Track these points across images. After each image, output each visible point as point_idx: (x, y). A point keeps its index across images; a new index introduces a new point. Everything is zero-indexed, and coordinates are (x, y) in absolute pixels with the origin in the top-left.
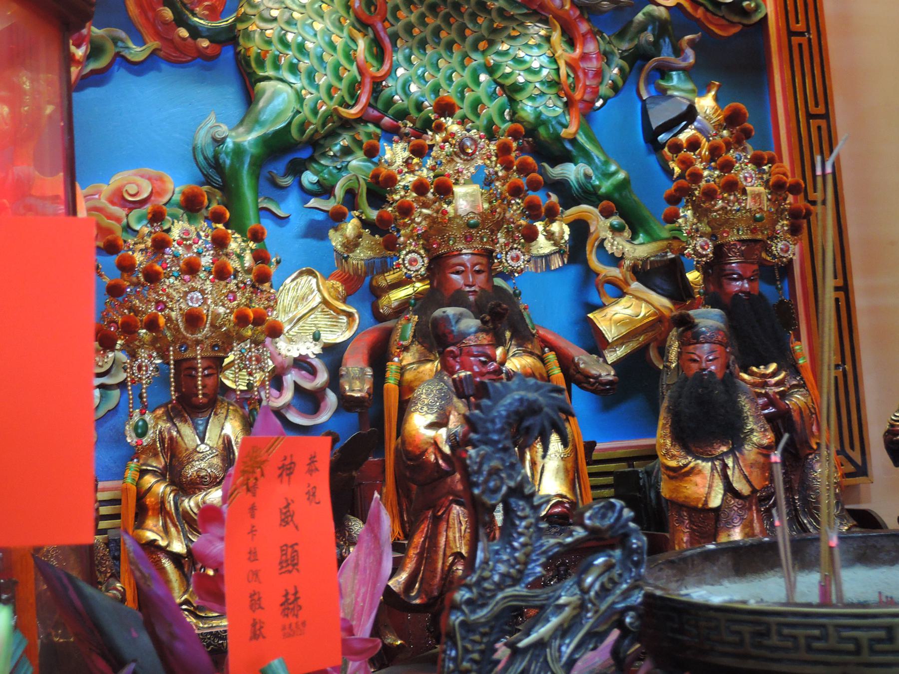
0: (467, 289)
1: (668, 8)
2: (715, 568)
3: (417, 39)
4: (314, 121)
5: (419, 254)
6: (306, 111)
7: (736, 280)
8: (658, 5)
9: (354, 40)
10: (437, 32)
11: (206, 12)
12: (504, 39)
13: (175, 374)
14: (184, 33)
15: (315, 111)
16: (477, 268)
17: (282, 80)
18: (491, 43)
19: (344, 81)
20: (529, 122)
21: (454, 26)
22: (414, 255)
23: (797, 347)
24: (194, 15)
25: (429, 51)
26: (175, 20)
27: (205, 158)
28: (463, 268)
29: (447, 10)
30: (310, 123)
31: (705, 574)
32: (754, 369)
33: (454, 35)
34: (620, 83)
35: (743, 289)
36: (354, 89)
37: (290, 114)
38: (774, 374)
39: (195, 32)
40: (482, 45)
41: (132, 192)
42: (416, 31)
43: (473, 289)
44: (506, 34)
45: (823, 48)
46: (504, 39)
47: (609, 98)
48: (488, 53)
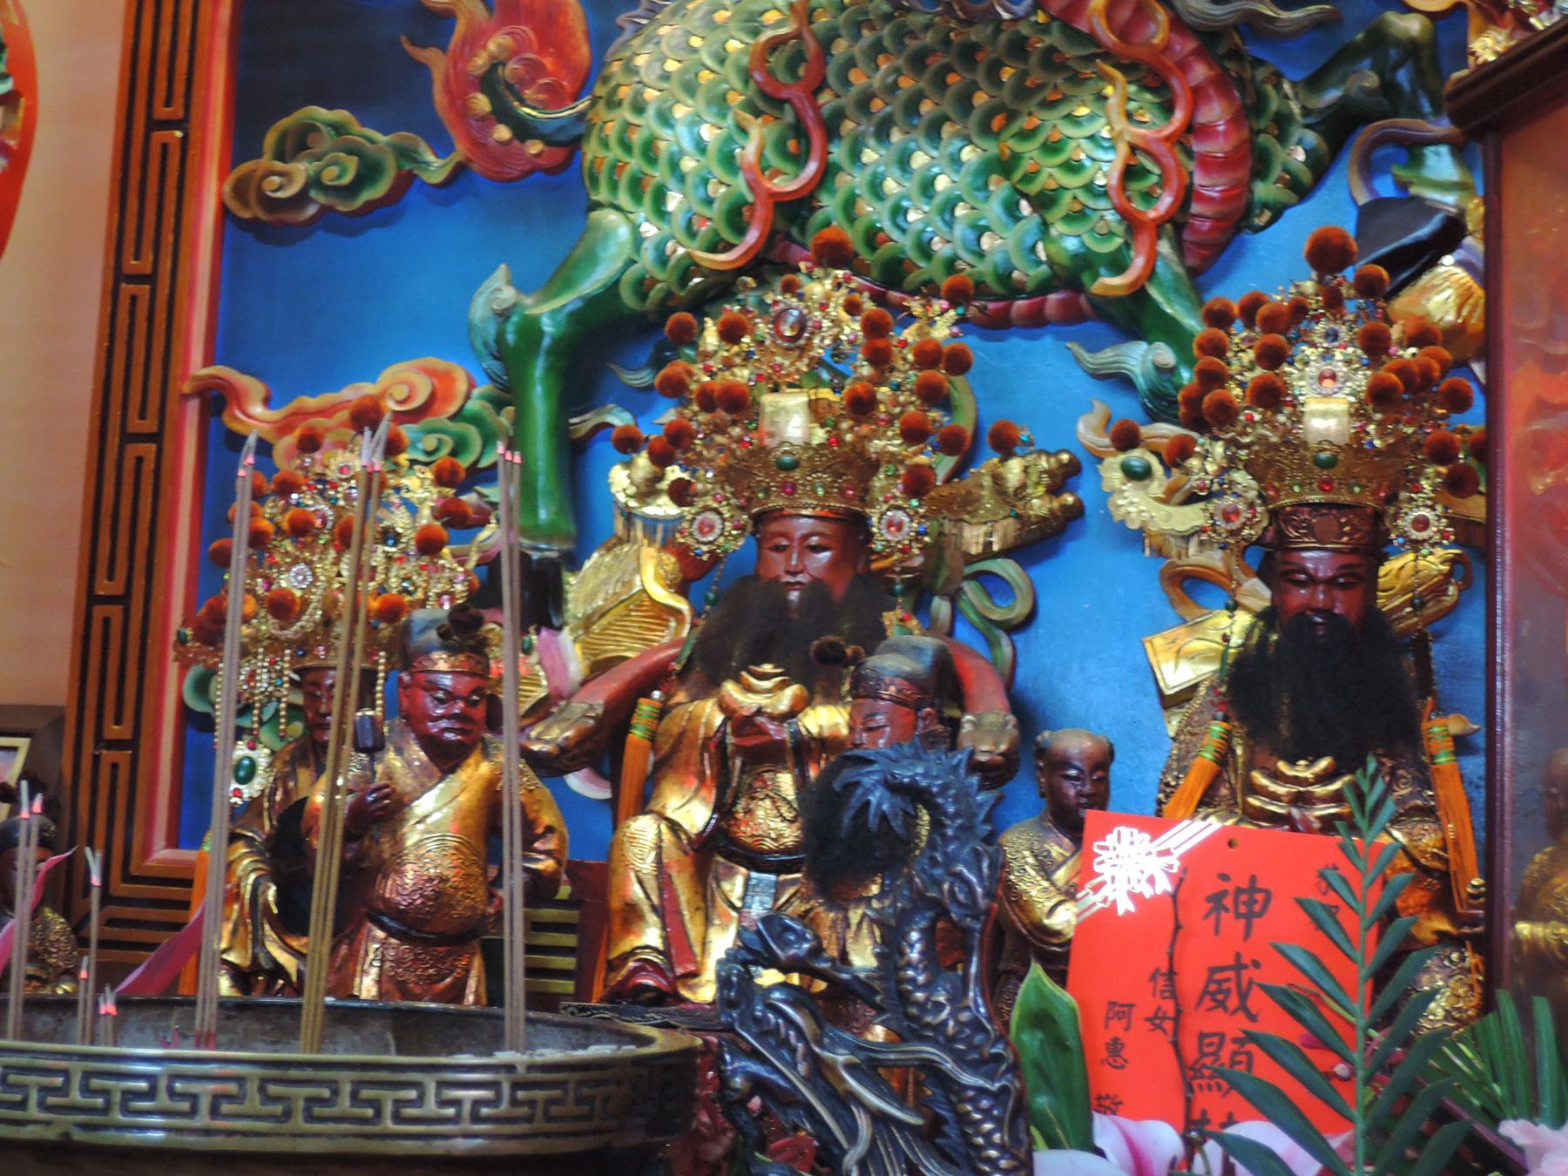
0: (790, 579)
1: (1432, 16)
2: (357, 1038)
3: (875, 119)
4: (661, 276)
5: (720, 514)
6: (647, 258)
7: (1301, 584)
8: (1411, 10)
9: (743, 131)
10: (912, 107)
11: (542, 97)
12: (1033, 109)
13: (375, 685)
14: (503, 132)
15: (662, 260)
16: (815, 540)
17: (618, 208)
18: (1012, 116)
19: (716, 205)
20: (1061, 265)
21: (950, 92)
22: (712, 516)
23: (1436, 730)
24: (523, 102)
25: (896, 136)
26: (493, 112)
27: (486, 344)
28: (785, 542)
29: (946, 60)
30: (655, 281)
31: (335, 1043)
32: (1282, 766)
33: (947, 107)
34: (1306, 176)
35: (1313, 605)
36: (737, 217)
37: (619, 265)
38: (1324, 778)
39: (524, 130)
40: (997, 122)
41: (401, 397)
42: (877, 104)
43: (800, 578)
44: (1038, 98)
45: (113, 246)
46: (1033, 109)
47: (1286, 206)
48: (1005, 135)
